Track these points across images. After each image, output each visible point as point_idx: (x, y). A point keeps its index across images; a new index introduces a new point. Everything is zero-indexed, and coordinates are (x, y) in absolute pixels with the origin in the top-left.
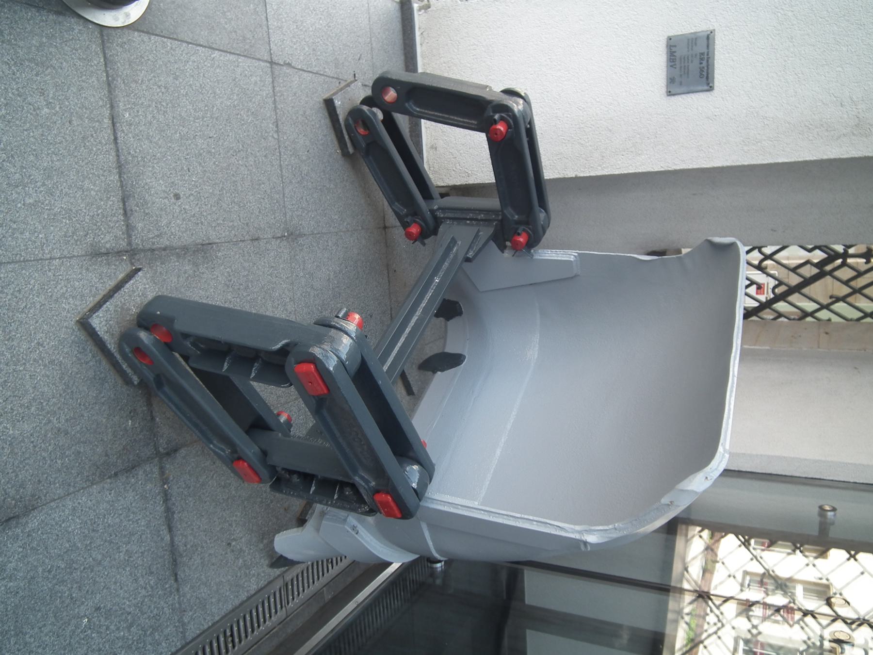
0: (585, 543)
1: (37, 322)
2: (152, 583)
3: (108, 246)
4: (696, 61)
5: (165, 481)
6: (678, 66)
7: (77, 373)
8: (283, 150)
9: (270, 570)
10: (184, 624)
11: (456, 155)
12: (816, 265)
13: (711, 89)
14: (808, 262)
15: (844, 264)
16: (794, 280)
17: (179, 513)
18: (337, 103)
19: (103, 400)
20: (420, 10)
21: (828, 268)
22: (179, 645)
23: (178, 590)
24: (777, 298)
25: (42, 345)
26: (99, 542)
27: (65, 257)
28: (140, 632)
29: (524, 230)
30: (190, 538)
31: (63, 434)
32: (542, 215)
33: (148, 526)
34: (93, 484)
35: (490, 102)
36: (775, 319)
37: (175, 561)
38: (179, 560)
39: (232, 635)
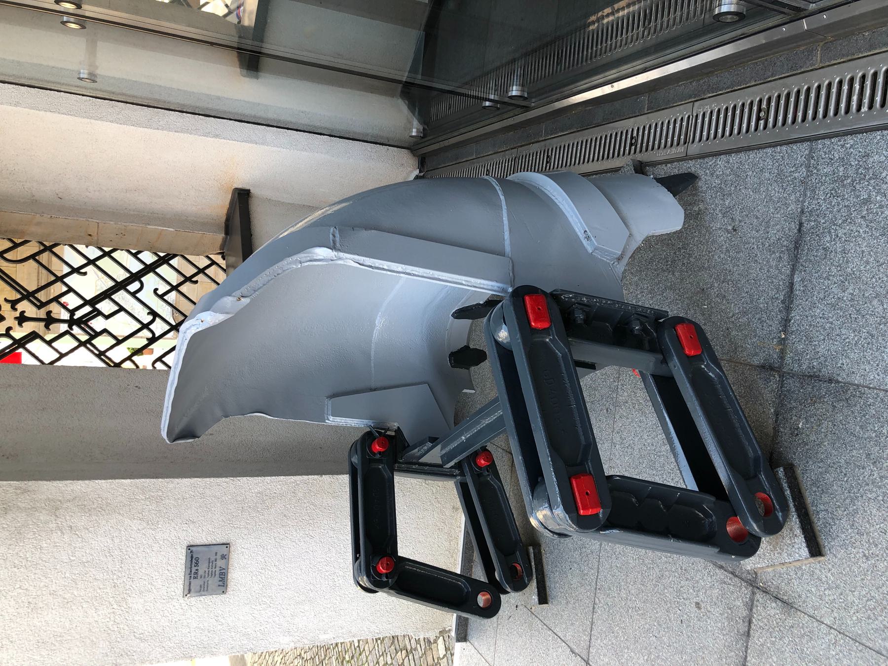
0: (333, 248)
1: (863, 579)
2: (828, 238)
3: (774, 605)
4: (201, 572)
5: (782, 342)
6: (218, 569)
7: (839, 507)
8: (594, 584)
9: (700, 173)
10: (808, 167)
11: (431, 524)
12: (100, 313)
13: (189, 547)
14: (107, 317)
15: (72, 312)
16: (121, 297)
17: (777, 298)
18: (535, 598)
19: (821, 465)
20: (450, 630)
21: (87, 309)
22: (820, 144)
23: (802, 212)
24: (136, 277)
25: (865, 556)
26: (871, 320)
27: (817, 621)
28: (858, 187)
29: (374, 454)
30: (774, 263)
31: (872, 457)
32: (355, 459)
33: (814, 306)
34: (858, 386)
35: (391, 588)
36: (139, 252)
37: (796, 248)
38: (792, 246)
39: (758, 119)
